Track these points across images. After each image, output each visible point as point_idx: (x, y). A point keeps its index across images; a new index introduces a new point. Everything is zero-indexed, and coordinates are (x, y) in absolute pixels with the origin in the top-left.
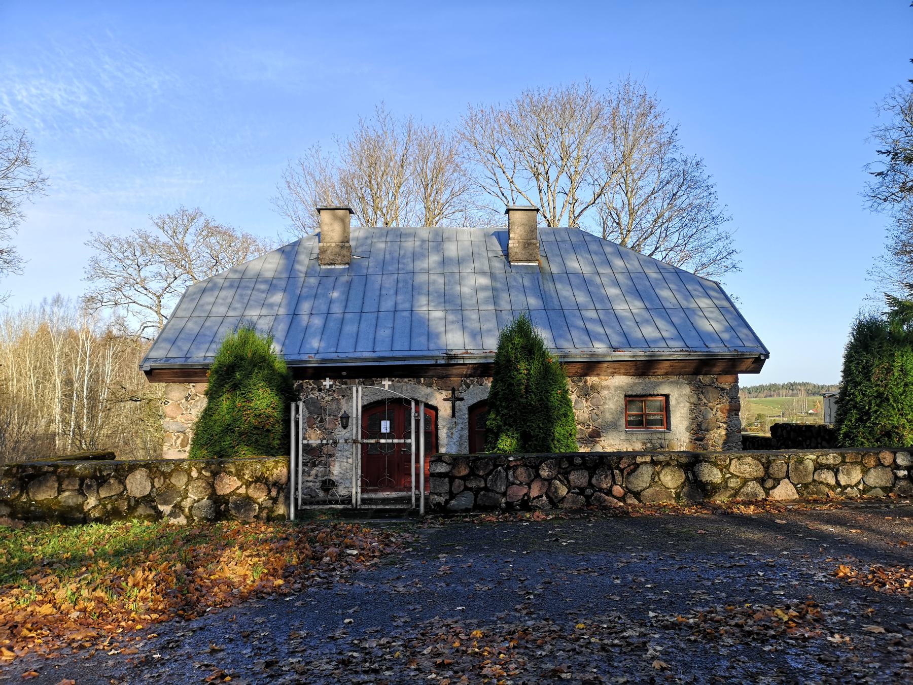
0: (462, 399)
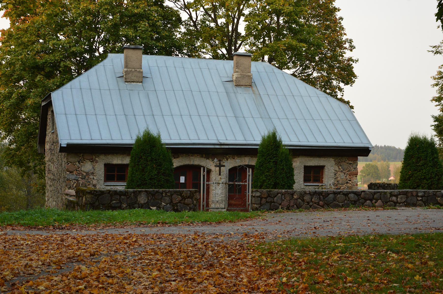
0: (224, 166)
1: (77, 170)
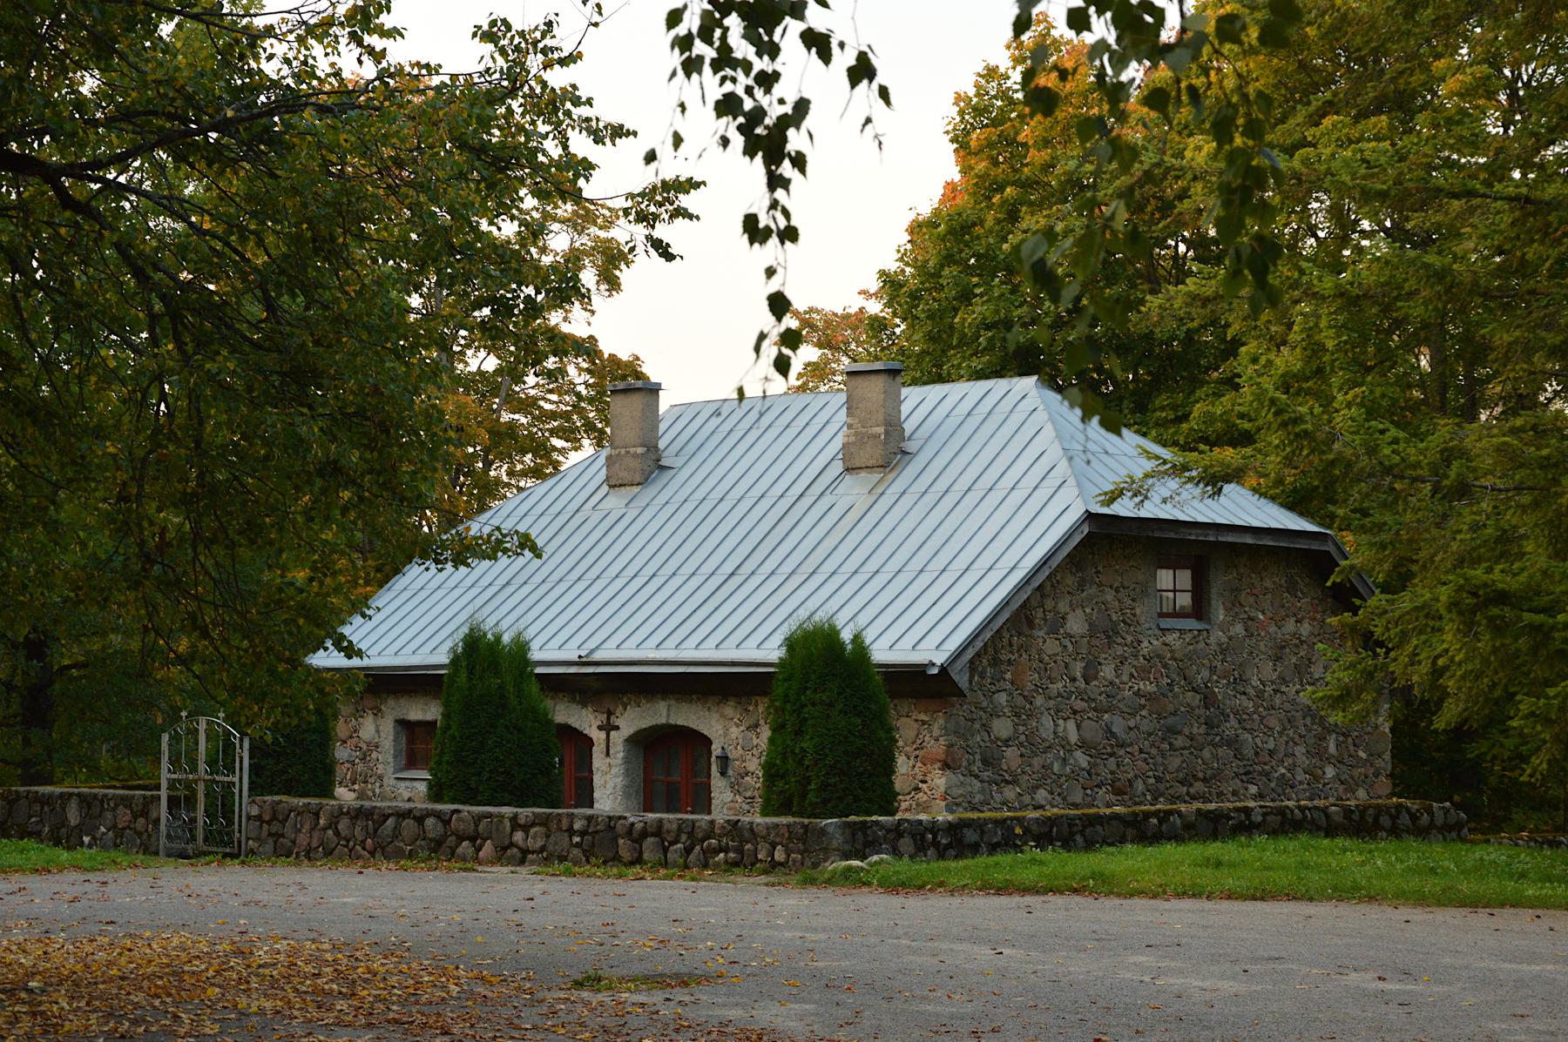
0: (617, 728)
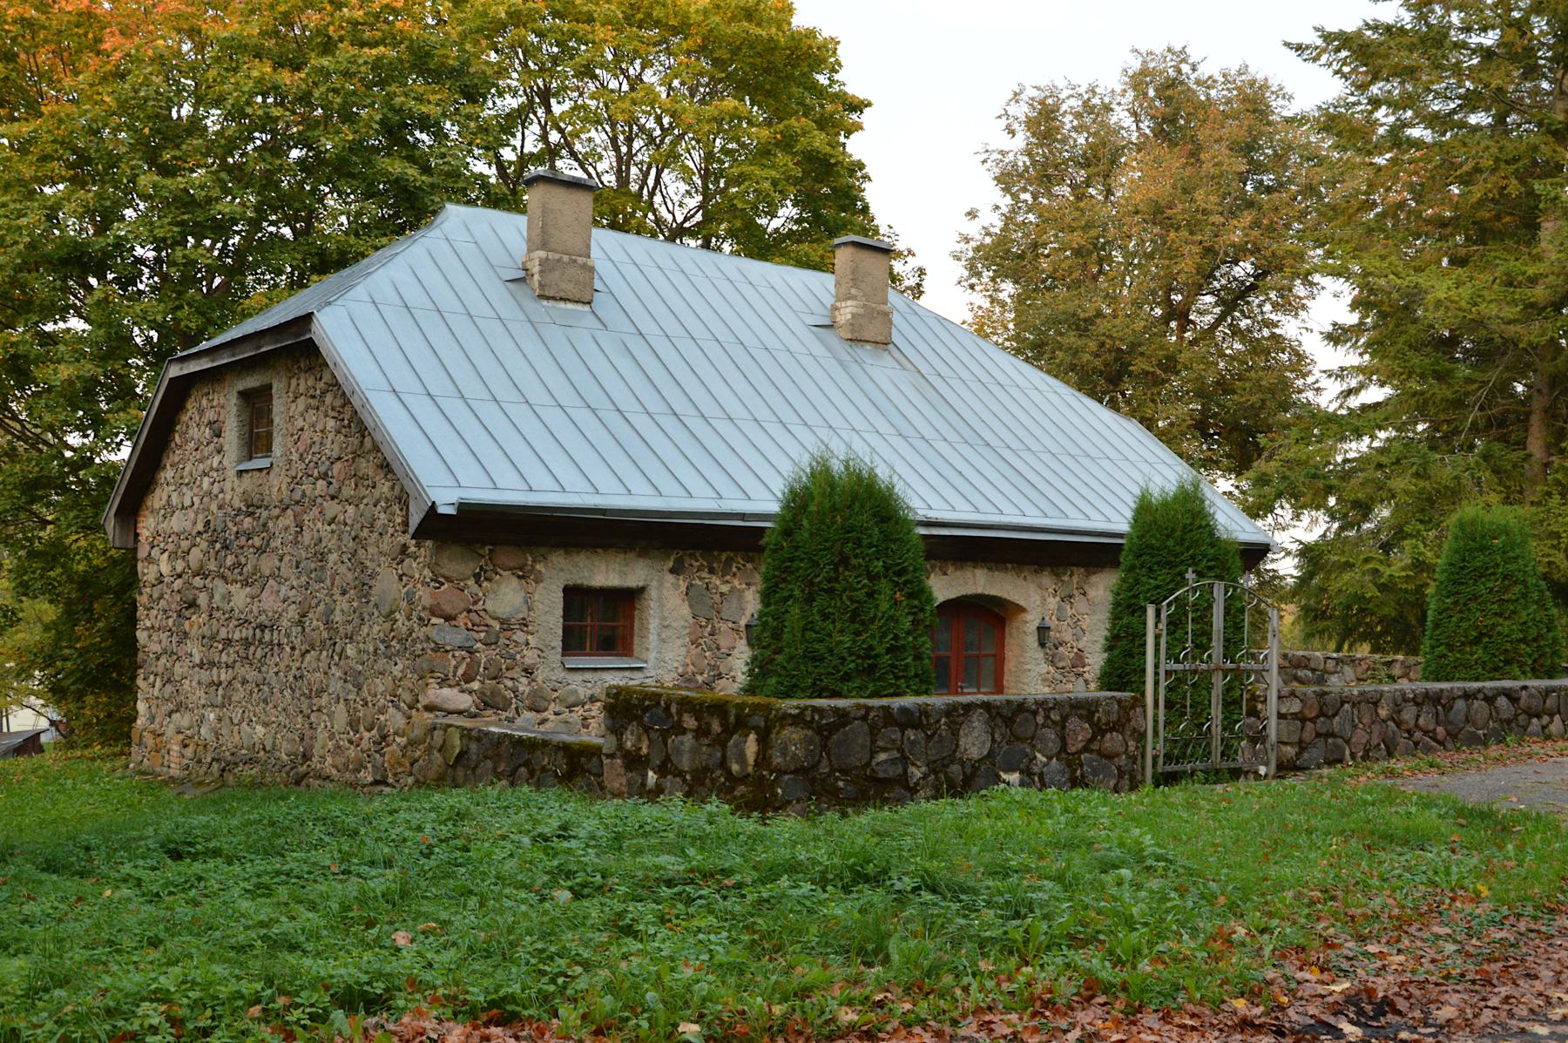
1: (469, 611)
